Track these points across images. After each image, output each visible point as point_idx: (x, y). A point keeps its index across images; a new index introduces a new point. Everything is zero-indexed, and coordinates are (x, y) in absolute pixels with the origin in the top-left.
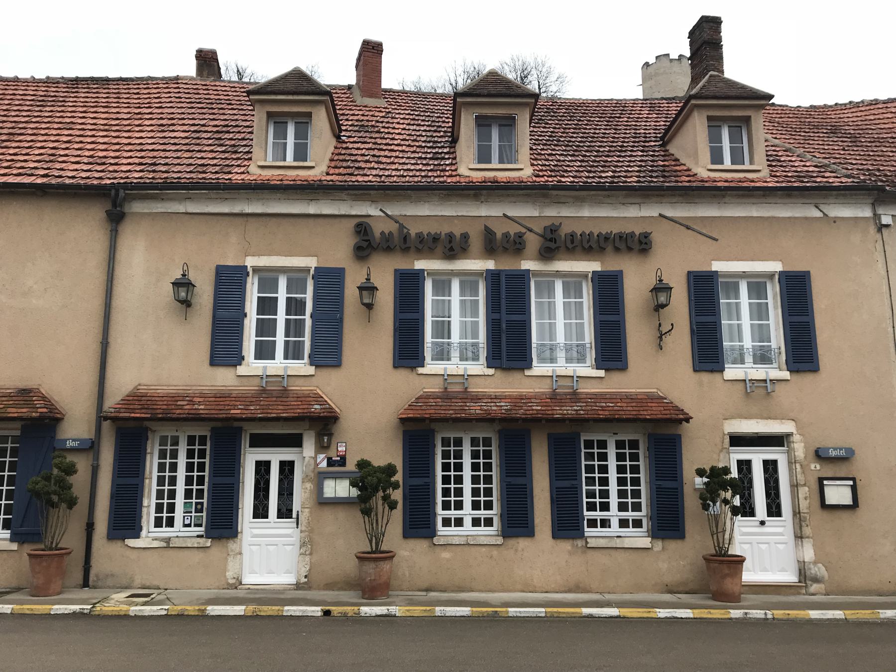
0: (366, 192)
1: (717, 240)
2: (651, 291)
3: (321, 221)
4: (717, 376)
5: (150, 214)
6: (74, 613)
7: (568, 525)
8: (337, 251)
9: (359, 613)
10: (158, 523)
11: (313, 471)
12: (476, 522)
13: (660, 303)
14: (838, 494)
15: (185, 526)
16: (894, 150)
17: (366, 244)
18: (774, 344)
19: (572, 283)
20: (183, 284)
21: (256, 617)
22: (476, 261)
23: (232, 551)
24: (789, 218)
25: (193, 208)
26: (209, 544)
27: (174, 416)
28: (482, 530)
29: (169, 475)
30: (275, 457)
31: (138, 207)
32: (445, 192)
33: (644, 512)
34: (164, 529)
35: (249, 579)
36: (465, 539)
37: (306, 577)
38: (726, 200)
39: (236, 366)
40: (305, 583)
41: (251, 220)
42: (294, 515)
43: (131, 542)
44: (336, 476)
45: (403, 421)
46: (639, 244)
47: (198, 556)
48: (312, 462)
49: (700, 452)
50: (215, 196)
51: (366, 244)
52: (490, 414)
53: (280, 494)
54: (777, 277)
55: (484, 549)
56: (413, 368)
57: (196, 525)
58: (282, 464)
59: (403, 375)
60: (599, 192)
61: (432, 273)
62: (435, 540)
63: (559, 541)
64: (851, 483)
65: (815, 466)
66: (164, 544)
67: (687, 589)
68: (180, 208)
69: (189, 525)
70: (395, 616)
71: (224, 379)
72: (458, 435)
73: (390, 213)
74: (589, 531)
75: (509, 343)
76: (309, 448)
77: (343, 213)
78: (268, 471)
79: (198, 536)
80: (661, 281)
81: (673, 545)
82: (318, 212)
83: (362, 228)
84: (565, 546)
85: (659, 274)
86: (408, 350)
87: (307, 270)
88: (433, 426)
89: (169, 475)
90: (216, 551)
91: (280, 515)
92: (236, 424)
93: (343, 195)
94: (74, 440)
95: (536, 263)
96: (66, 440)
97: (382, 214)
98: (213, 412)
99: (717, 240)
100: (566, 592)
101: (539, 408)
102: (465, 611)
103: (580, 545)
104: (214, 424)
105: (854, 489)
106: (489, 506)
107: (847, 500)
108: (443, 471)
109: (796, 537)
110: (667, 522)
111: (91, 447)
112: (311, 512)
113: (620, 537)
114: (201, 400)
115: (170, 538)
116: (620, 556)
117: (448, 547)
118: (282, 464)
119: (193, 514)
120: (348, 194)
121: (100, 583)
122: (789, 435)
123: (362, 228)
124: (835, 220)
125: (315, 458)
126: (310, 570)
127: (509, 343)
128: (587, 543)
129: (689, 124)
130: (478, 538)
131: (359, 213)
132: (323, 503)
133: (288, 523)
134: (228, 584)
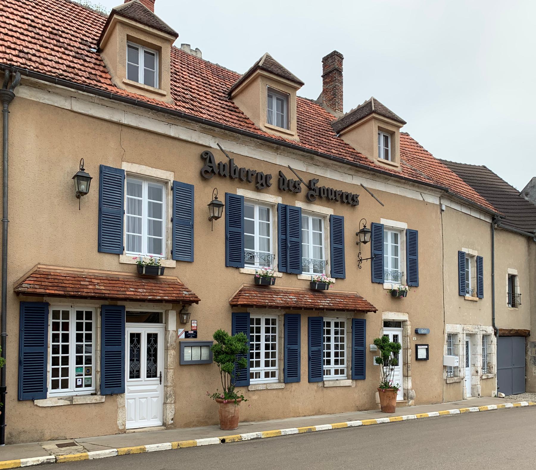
0: (212, 128)
1: (383, 206)
2: (74, 178)
3: (176, 143)
4: (381, 286)
5: (38, 103)
6: (42, 464)
7: (316, 374)
8: (190, 174)
9: (241, 439)
10: (55, 385)
12: (267, 375)
13: (80, 190)
15: (77, 386)
18: (399, 270)
19: (319, 220)
20: (81, 177)
21: (180, 449)
22: (273, 196)
23: (120, 404)
24: (411, 198)
25: (78, 107)
26: (103, 400)
27: (84, 294)
28: (270, 380)
29: (75, 345)
30: (144, 329)
31: (23, 93)
32: (260, 141)
33: (345, 366)
34: (270, 378)
35: (129, 425)
36: (265, 386)
37: (172, 420)
38: (389, 182)
39: (297, 275)
40: (171, 424)
41: (125, 129)
42: (158, 375)
43: (40, 403)
44: (192, 346)
45: (233, 306)
46: (350, 200)
47: (95, 410)
48: (174, 334)
49: (374, 331)
50: (98, 102)
51: (211, 168)
52: (288, 304)
53: (131, 360)
54: (405, 232)
55: (275, 392)
56: (237, 268)
57: (86, 386)
58: (149, 335)
59: (231, 272)
60: (338, 163)
61: (392, 228)
62: (250, 388)
63: (311, 384)
64: (426, 347)
65: (415, 338)
66: (68, 403)
67: (365, 408)
68: (66, 104)
69: (81, 386)
70: (261, 438)
71: (108, 265)
73: (223, 148)
74: (326, 378)
75: (290, 258)
76: (172, 324)
77: (194, 141)
78: (139, 342)
79: (92, 394)
80: (216, 198)
81: (360, 383)
82: (177, 136)
83: (206, 157)
84: (314, 386)
85: (215, 192)
86: (236, 255)
87: (166, 183)
88: (249, 310)
89: (75, 345)
90: (109, 404)
92: (120, 303)
93: (197, 126)
95: (303, 204)
97: (218, 148)
98: (113, 292)
99: (383, 206)
100: (314, 415)
101: (310, 301)
102: (295, 430)
103: (320, 386)
104: (102, 302)
105: (427, 350)
106: (273, 364)
107: (420, 357)
108: (53, 330)
109: (404, 376)
110: (358, 371)
112: (174, 373)
113: (337, 380)
114: (99, 281)
115: (72, 397)
116: (339, 391)
117: (257, 392)
118: (149, 335)
119: (84, 377)
120: (200, 127)
121: (14, 439)
122: (405, 321)
123: (206, 157)
124: (427, 203)
125: (177, 331)
126: (175, 414)
127: (290, 258)
128: (324, 384)
129: (366, 127)
130: (272, 385)
131: (204, 144)
132: (182, 364)
134: (119, 430)
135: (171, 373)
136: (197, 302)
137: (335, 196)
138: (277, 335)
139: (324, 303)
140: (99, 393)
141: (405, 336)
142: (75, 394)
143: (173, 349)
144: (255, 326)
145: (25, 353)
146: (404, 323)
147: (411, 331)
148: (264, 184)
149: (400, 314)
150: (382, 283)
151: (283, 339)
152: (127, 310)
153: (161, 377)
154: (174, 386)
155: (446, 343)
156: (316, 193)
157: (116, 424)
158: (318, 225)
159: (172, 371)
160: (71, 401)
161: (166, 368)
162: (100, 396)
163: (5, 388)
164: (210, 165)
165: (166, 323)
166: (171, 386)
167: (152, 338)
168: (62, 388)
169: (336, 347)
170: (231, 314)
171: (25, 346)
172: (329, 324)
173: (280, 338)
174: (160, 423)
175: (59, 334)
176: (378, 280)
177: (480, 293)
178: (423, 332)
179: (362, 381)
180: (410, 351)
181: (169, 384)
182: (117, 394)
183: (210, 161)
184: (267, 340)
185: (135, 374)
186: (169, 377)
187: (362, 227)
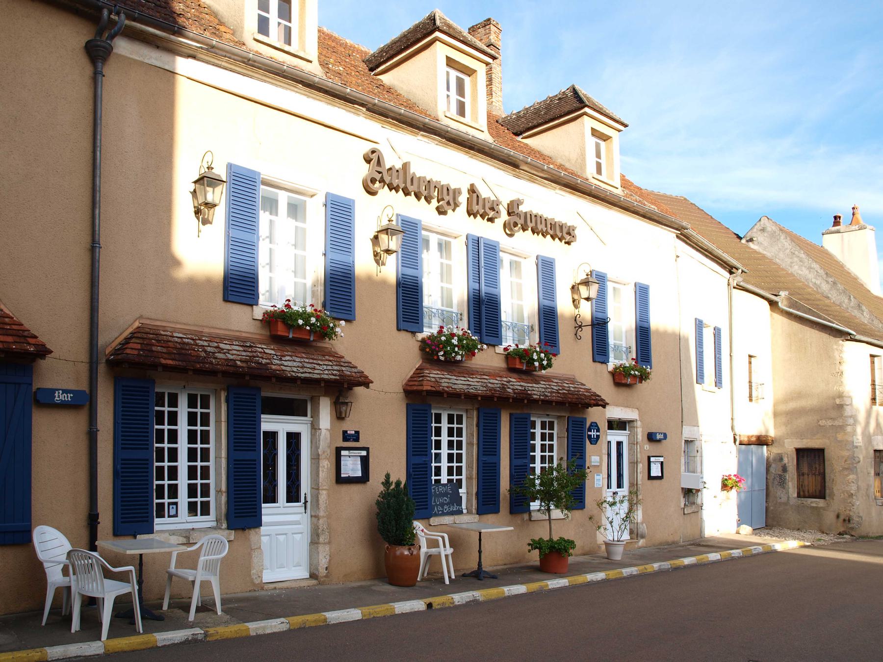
4: (604, 365)
8: (349, 181)
11: (329, 447)
14: (656, 471)
16: (1, 326)
17: (381, 177)
34: (199, 518)
35: (268, 576)
39: (252, 305)
63: (485, 516)
65: (647, 446)
72: (294, 428)
83: (373, 158)
91: (289, 500)
94: (65, 391)
96: (53, 391)
111: (83, 402)
112: (329, 495)
122: (631, 421)
123: (373, 158)
126: (330, 560)
133: (297, 507)
135: (323, 496)
136: (366, 383)
137: (546, 226)
138: (464, 439)
139: (537, 390)
140: (224, 526)
141: (633, 443)
142: (190, 526)
143: (326, 458)
144: (166, 409)
145: (122, 460)
146: (632, 424)
147: (642, 436)
148: (452, 202)
149: (628, 410)
150: (605, 362)
151: (475, 447)
152: (264, 394)
153: (306, 502)
154: (329, 517)
155: (683, 454)
156: (520, 220)
157: (250, 575)
158: (444, 247)
159: (324, 492)
160: (188, 538)
161: (316, 488)
162: (228, 531)
163: (98, 515)
164: (379, 169)
165: (316, 415)
166: (323, 517)
167: (293, 439)
168: (202, 515)
169: (450, 458)
170: (405, 406)
171: (123, 448)
172: (438, 419)
173: (470, 444)
174: (306, 575)
175: (201, 431)
176: (601, 358)
177: (718, 383)
178: (659, 437)
179: (580, 511)
180: (640, 466)
181: (321, 514)
182: (250, 528)
183: (379, 163)
184: (543, 450)
185: (272, 498)
186: (321, 502)
187: (385, 223)
